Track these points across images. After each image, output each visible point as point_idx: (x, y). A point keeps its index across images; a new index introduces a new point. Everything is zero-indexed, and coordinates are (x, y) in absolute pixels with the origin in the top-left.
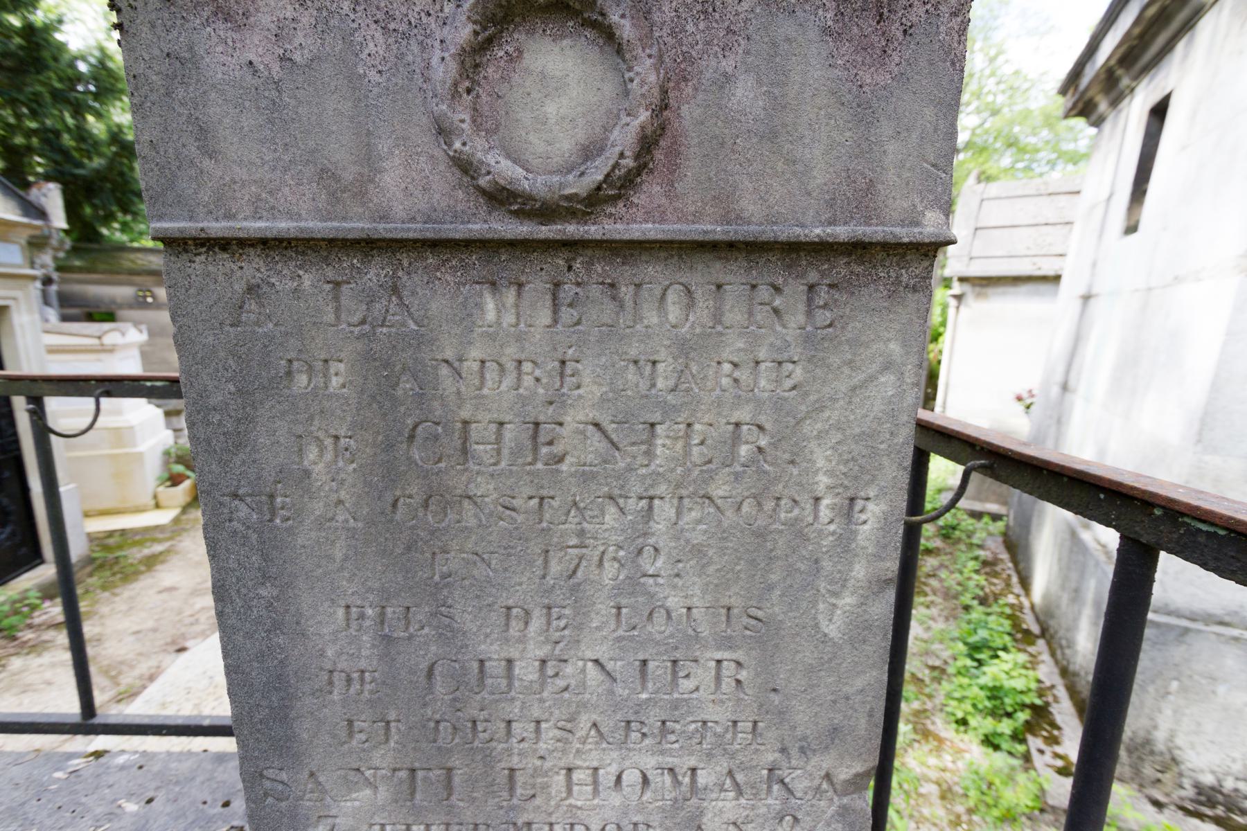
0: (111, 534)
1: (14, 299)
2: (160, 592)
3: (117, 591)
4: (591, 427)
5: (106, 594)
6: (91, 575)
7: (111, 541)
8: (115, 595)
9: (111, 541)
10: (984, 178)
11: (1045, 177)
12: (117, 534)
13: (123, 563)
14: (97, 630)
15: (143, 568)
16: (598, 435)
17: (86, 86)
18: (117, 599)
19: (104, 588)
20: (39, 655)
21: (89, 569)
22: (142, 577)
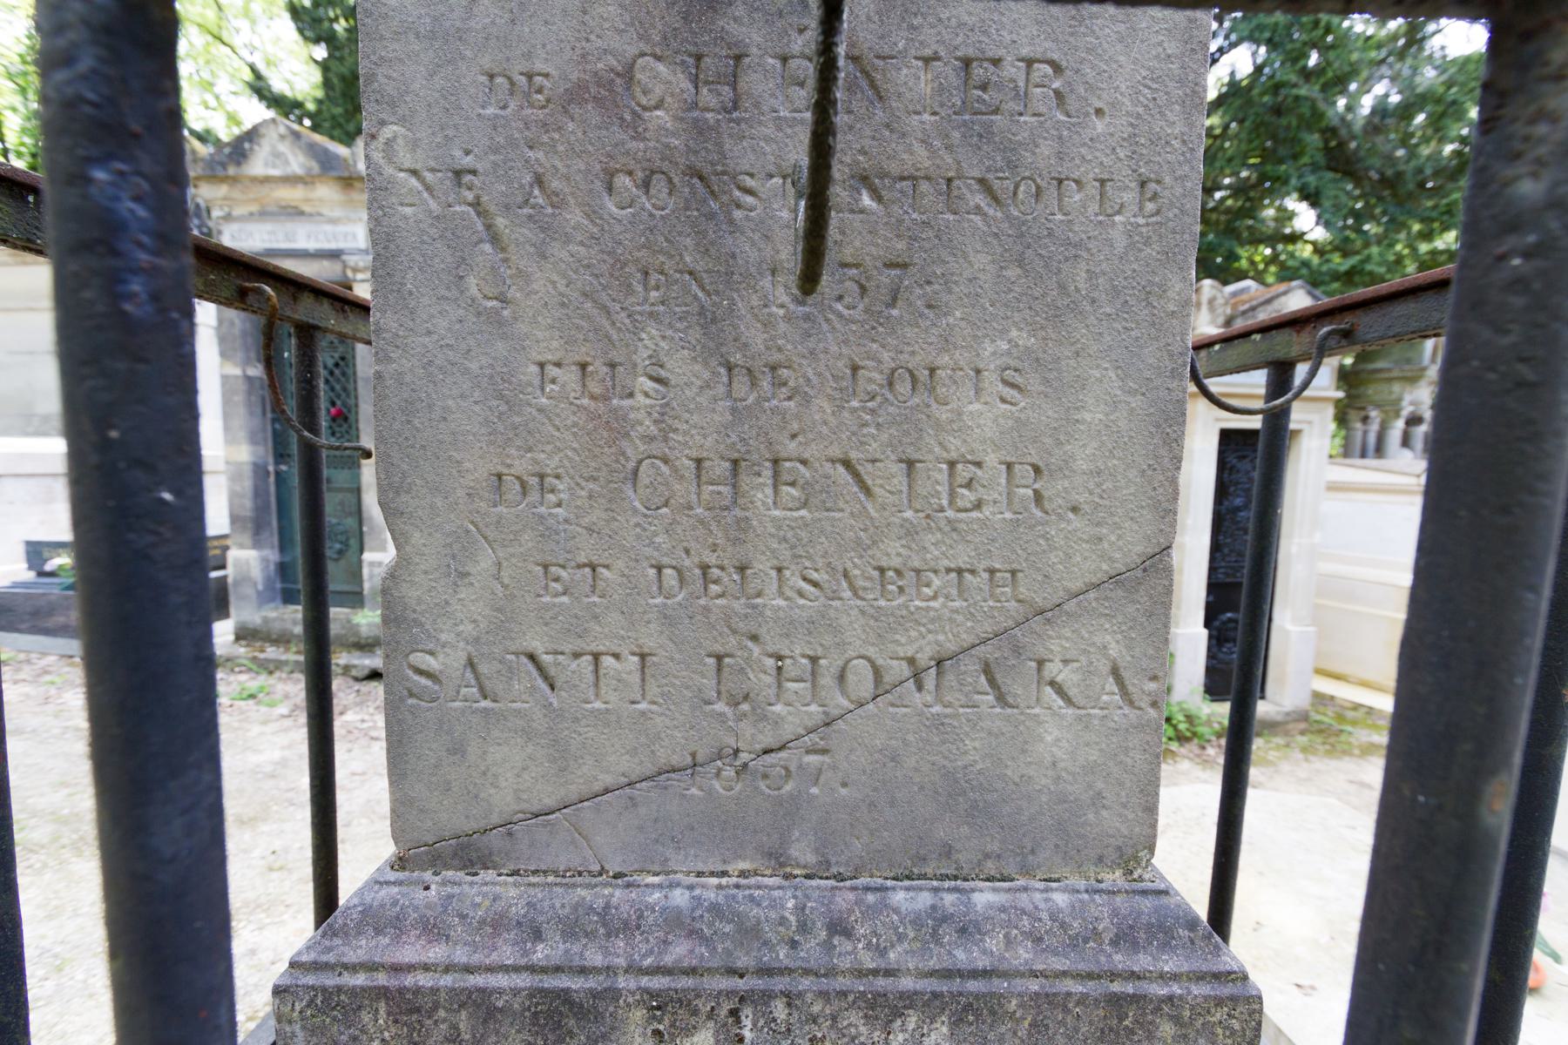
0: (1356, 707)
1: (1310, 422)
2: (1351, 782)
3: (1312, 758)
4: (524, 660)
5: (1301, 756)
6: (1302, 733)
7: (1350, 714)
8: (1307, 760)
9: (1350, 714)
10: (16, 682)
11: (551, 647)
12: (1363, 710)
13: (1343, 738)
14: (1262, 779)
15: (1357, 752)
16: (531, 667)
17: (1236, 174)
18: (1305, 765)
19: (1304, 750)
20: (1204, 769)
21: (1303, 726)
22: (1347, 758)
